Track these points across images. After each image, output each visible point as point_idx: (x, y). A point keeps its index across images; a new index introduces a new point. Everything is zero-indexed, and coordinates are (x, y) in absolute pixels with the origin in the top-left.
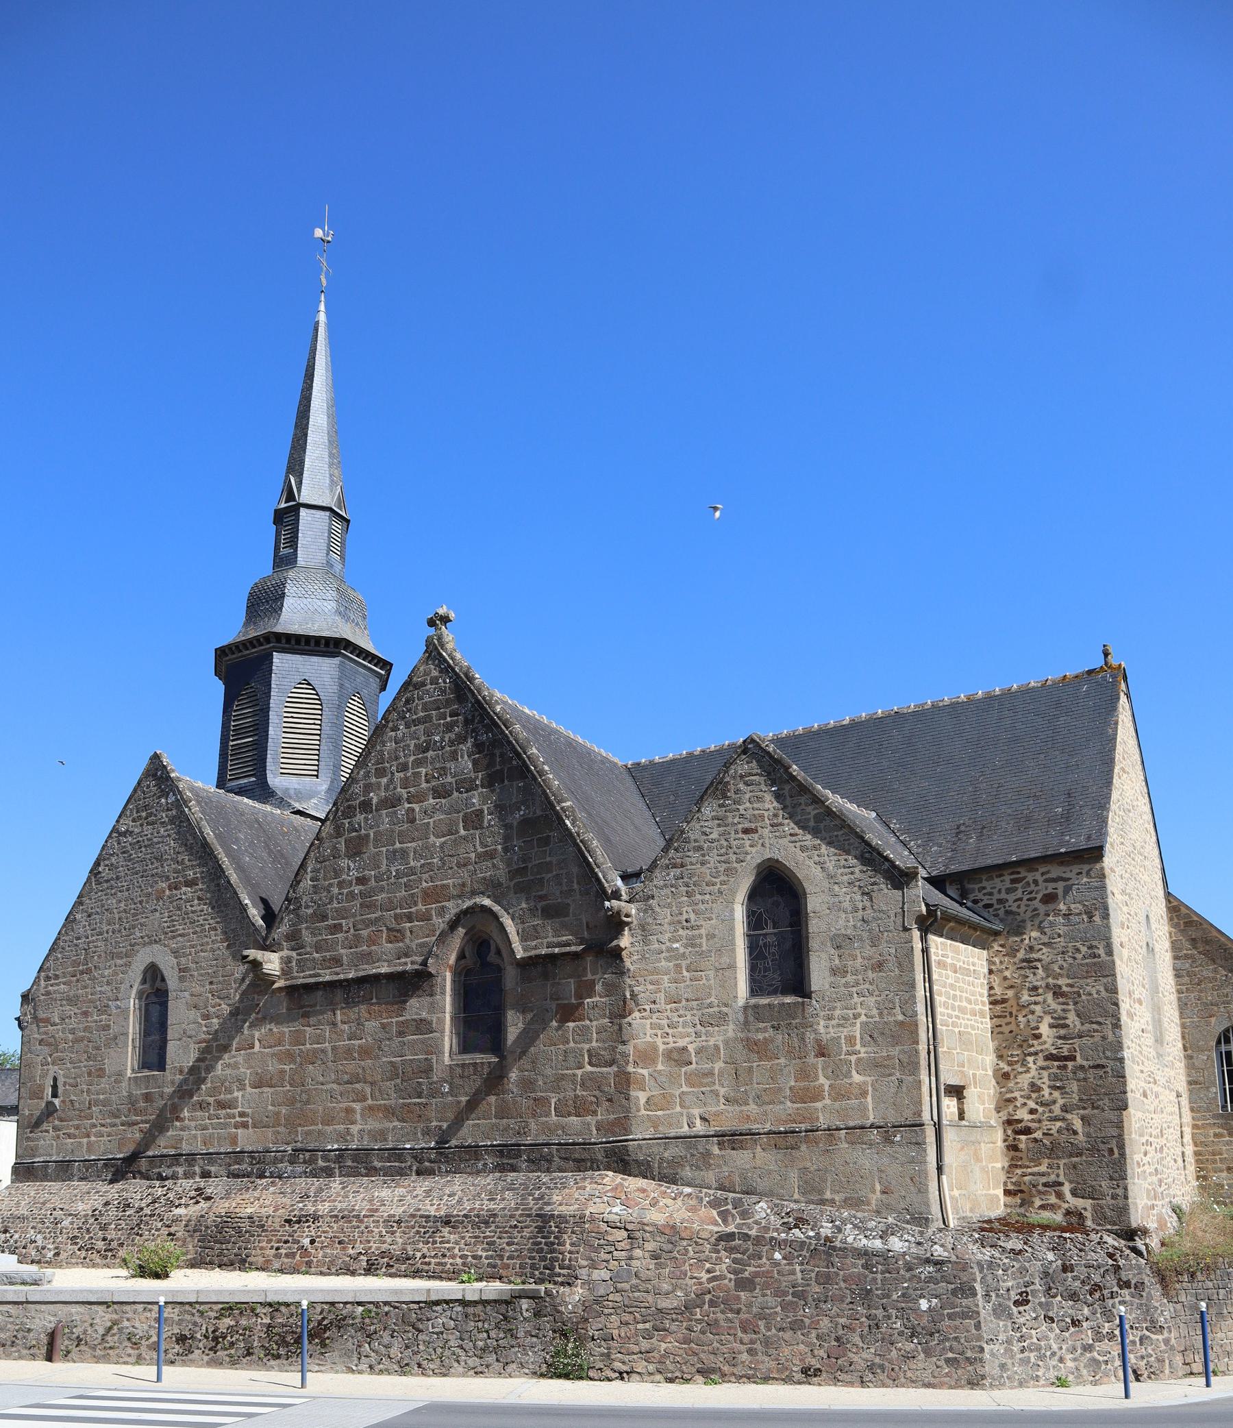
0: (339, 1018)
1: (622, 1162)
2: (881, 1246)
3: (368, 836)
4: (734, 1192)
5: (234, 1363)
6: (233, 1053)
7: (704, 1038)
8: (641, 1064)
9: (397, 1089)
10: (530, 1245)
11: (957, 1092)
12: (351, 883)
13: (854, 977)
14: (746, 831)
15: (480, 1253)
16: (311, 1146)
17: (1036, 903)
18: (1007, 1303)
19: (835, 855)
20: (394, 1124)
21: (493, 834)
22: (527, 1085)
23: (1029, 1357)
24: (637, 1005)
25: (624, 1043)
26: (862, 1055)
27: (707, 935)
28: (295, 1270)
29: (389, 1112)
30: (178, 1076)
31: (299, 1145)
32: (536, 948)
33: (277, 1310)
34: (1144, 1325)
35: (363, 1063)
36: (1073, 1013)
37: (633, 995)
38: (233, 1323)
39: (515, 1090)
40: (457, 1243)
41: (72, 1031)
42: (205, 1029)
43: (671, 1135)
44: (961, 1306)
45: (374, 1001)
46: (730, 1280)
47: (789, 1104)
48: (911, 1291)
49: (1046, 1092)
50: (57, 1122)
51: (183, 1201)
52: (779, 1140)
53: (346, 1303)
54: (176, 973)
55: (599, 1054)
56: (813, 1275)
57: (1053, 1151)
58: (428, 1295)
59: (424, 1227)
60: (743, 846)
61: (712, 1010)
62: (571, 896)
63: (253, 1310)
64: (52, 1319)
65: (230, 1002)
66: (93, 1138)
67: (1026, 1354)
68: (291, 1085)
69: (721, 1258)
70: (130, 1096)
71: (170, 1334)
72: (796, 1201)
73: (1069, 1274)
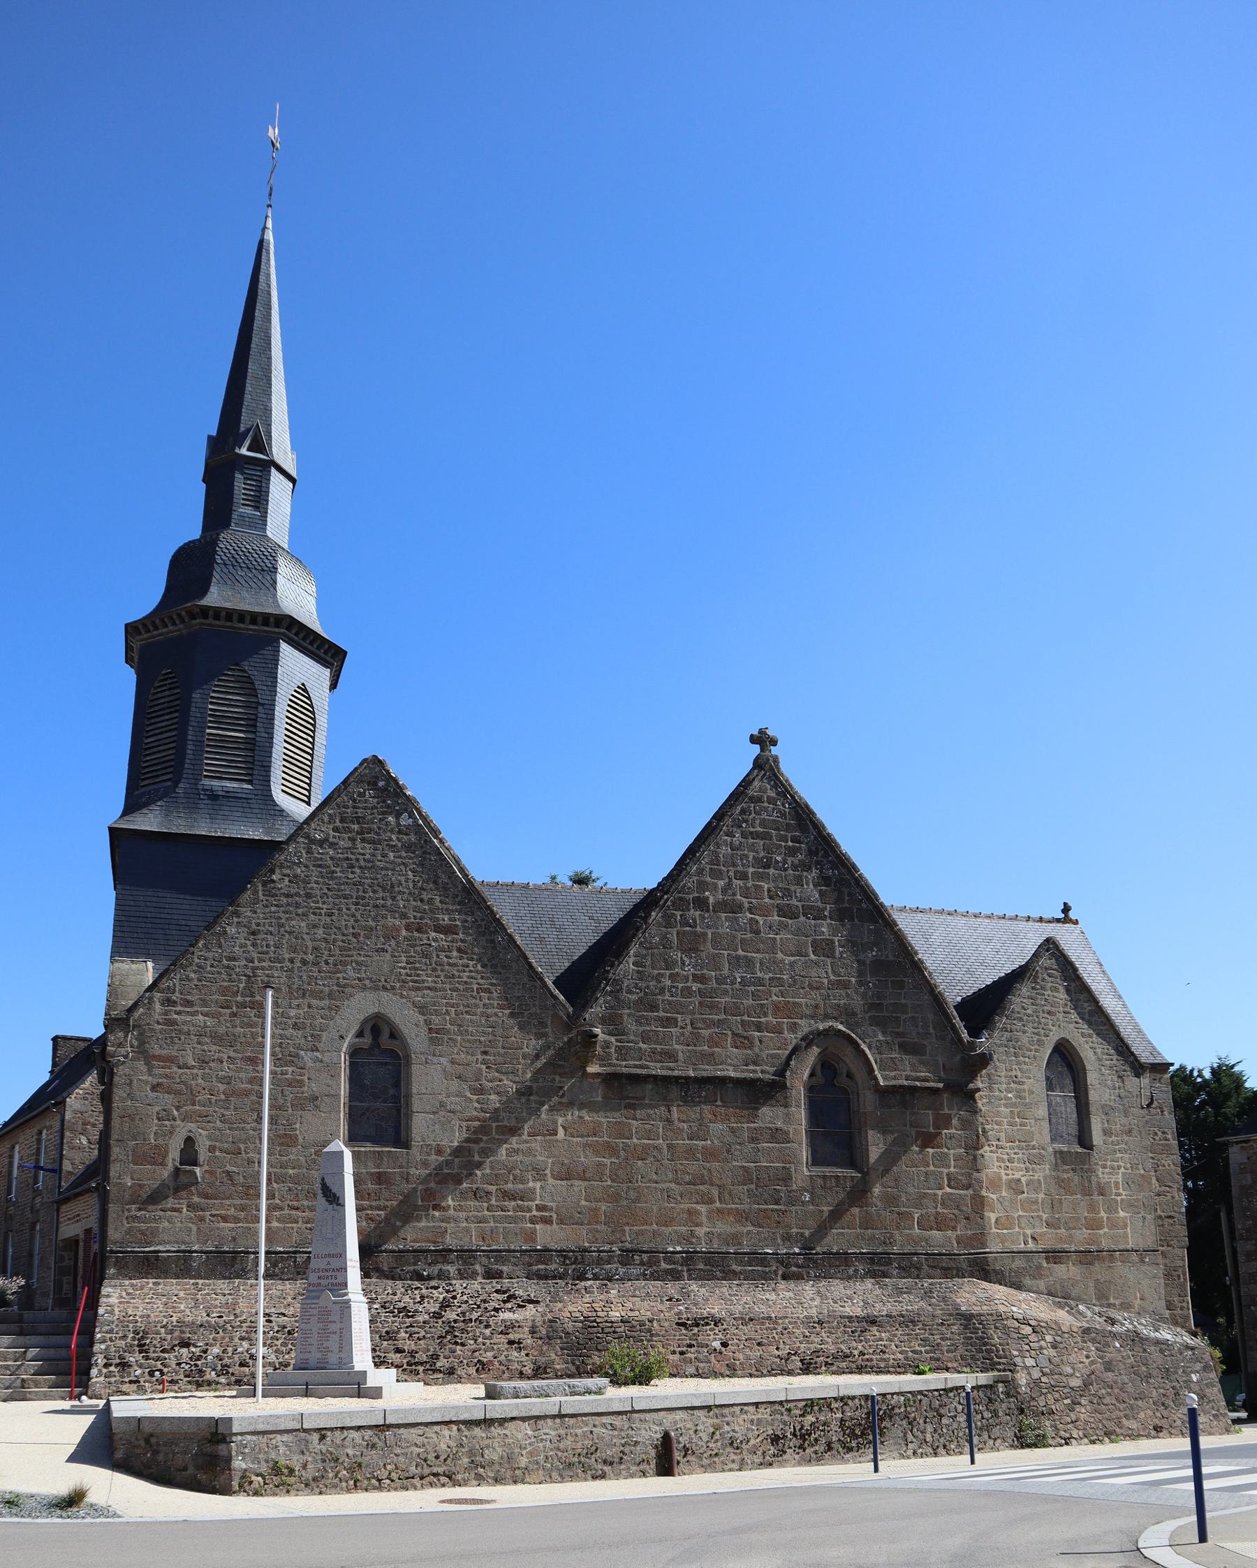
0: (675, 1115)
1: (983, 1270)
3: (705, 934)
4: (1058, 1297)
5: (818, 1459)
6: (525, 1137)
8: (992, 1190)
9: (750, 1194)
15: (917, 1348)
19: (1101, 1044)
20: (748, 1228)
21: (845, 966)
22: (891, 1201)
24: (988, 1140)
25: (978, 1171)
28: (715, 1374)
29: (743, 1217)
30: (434, 1157)
31: (628, 1245)
32: (895, 1078)
33: (846, 1404)
35: (708, 1165)
37: (984, 1131)
38: (814, 1420)
39: (878, 1204)
41: (227, 1080)
42: (476, 1105)
45: (719, 1103)
50: (196, 1199)
53: (893, 1394)
54: (424, 1031)
55: (957, 1179)
63: (829, 1406)
65: (517, 1079)
68: (613, 1181)
71: (765, 1435)
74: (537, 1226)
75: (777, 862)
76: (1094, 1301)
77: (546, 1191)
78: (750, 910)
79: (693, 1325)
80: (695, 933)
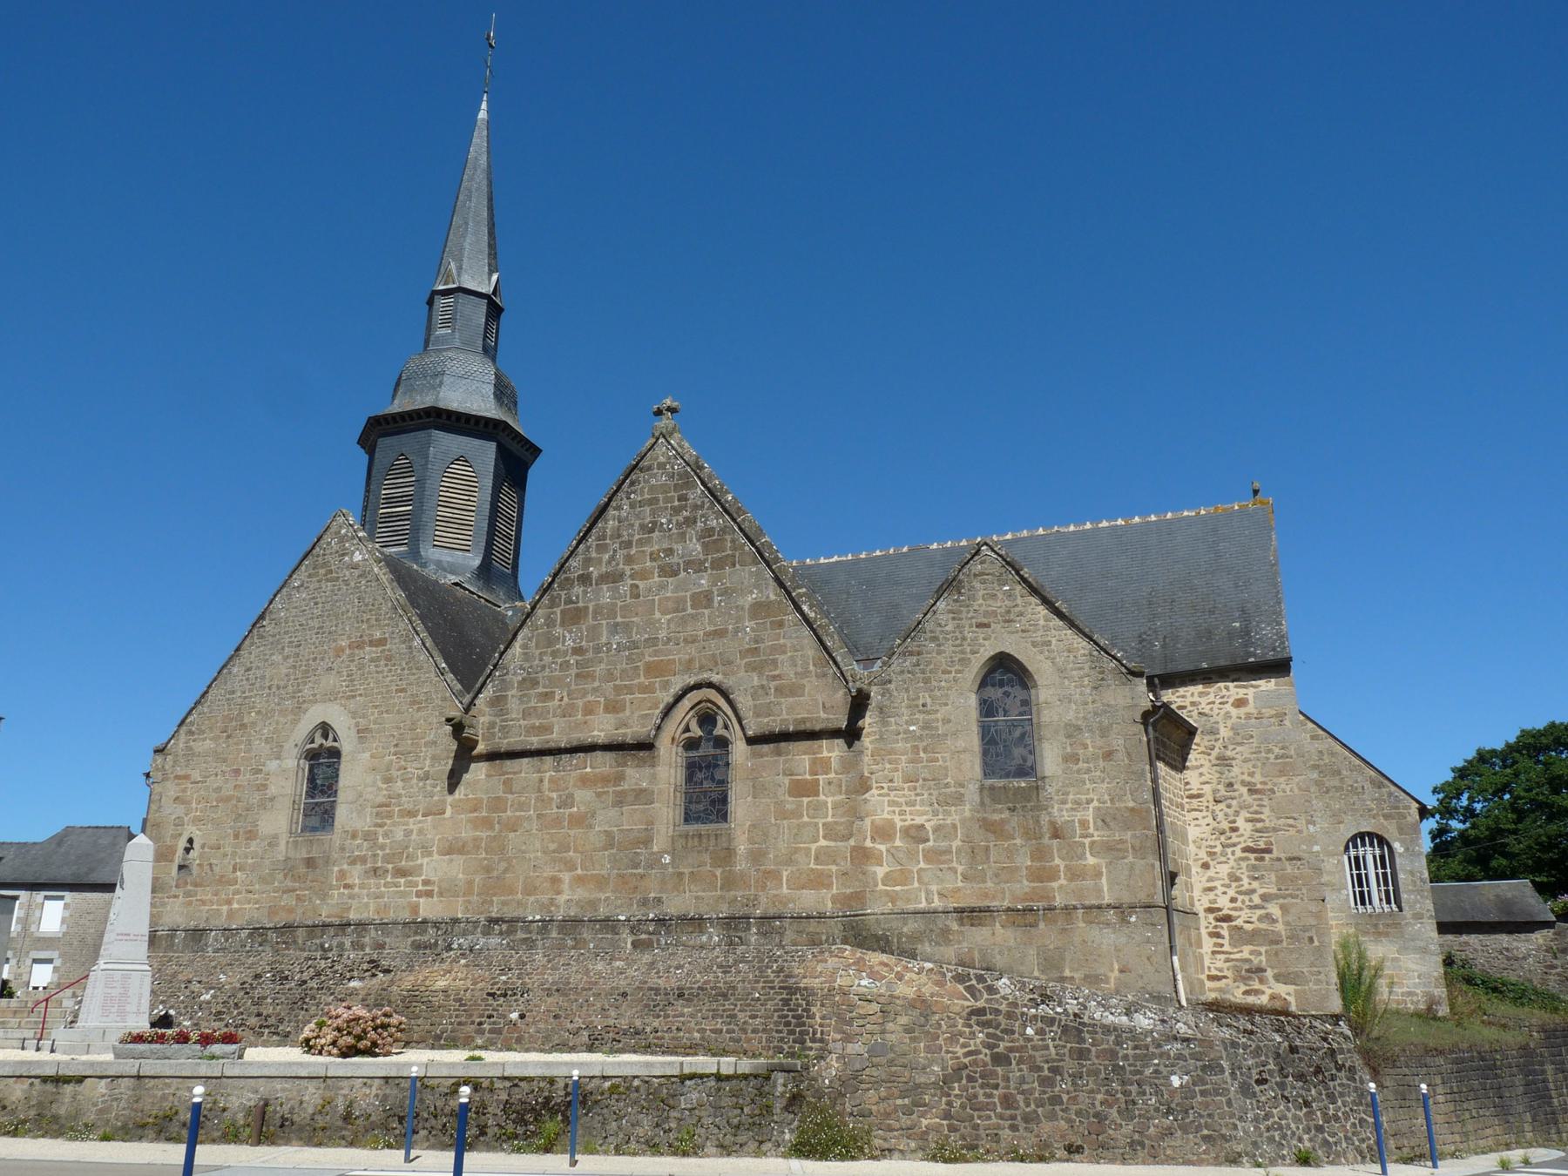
2: (1128, 1023)
3: (587, 608)
4: (974, 968)
8: (878, 840)
10: (775, 1018)
11: (400, 1024)
12: (565, 653)
13: (1085, 765)
16: (508, 916)
17: (1228, 707)
23: (1274, 1136)
26: (1096, 838)
31: (494, 915)
33: (516, 1085)
40: (692, 1016)
42: (385, 792)
46: (986, 1055)
48: (1162, 1068)
49: (1245, 881)
51: (355, 974)
52: (1019, 920)
53: (593, 1077)
54: (353, 733)
56: (1066, 1051)
58: (682, 1069)
59: (654, 1000)
60: (976, 639)
62: (807, 677)
64: (252, 1096)
66: (235, 906)
69: (974, 1033)
70: (287, 859)
72: (1037, 979)
73: (1296, 1056)
74: (421, 900)
75: (662, 524)
77: (433, 867)
78: (632, 577)
79: (501, 995)
80: (577, 609)
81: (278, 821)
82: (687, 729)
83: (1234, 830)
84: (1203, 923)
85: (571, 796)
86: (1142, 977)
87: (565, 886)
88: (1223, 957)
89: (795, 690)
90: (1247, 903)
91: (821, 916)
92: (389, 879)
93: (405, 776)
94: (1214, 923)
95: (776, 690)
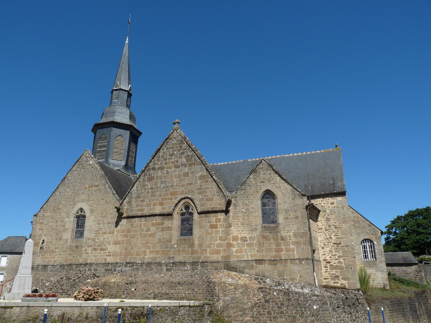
2: (302, 291)
4: (260, 276)
7: (251, 234)
11: (101, 292)
13: (290, 220)
14: (262, 182)
16: (132, 262)
18: (335, 307)
26: (293, 240)
27: (252, 208)
31: (128, 261)
33: (133, 309)
34: (365, 315)
36: (340, 232)
40: (182, 289)
42: (98, 227)
43: (243, 260)
44: (325, 308)
46: (263, 300)
47: (274, 252)
48: (311, 304)
49: (334, 252)
51: (89, 278)
53: (154, 307)
56: (285, 299)
57: (336, 267)
60: (261, 186)
61: (253, 227)
66: (56, 259)
67: (341, 321)
70: (70, 246)
72: (277, 279)
73: (347, 300)
74: (108, 257)
75: (175, 154)
76: (277, 278)
77: (111, 248)
78: (167, 168)
79: (130, 284)
81: (68, 235)
82: (182, 210)
83: (331, 238)
84: (322, 264)
85: (149, 228)
86: (306, 278)
87: (148, 253)
88: (328, 273)
89: (211, 200)
90: (334, 258)
91: (218, 262)
92: (99, 251)
93: (103, 223)
94: (325, 264)
95: (206, 199)
